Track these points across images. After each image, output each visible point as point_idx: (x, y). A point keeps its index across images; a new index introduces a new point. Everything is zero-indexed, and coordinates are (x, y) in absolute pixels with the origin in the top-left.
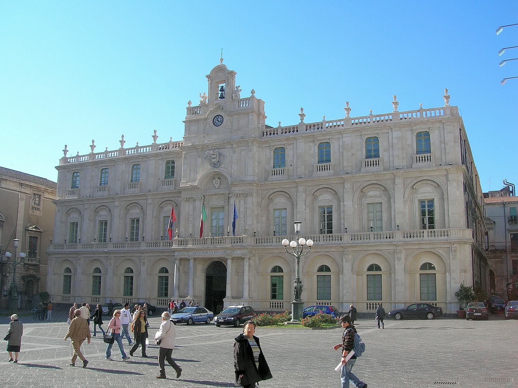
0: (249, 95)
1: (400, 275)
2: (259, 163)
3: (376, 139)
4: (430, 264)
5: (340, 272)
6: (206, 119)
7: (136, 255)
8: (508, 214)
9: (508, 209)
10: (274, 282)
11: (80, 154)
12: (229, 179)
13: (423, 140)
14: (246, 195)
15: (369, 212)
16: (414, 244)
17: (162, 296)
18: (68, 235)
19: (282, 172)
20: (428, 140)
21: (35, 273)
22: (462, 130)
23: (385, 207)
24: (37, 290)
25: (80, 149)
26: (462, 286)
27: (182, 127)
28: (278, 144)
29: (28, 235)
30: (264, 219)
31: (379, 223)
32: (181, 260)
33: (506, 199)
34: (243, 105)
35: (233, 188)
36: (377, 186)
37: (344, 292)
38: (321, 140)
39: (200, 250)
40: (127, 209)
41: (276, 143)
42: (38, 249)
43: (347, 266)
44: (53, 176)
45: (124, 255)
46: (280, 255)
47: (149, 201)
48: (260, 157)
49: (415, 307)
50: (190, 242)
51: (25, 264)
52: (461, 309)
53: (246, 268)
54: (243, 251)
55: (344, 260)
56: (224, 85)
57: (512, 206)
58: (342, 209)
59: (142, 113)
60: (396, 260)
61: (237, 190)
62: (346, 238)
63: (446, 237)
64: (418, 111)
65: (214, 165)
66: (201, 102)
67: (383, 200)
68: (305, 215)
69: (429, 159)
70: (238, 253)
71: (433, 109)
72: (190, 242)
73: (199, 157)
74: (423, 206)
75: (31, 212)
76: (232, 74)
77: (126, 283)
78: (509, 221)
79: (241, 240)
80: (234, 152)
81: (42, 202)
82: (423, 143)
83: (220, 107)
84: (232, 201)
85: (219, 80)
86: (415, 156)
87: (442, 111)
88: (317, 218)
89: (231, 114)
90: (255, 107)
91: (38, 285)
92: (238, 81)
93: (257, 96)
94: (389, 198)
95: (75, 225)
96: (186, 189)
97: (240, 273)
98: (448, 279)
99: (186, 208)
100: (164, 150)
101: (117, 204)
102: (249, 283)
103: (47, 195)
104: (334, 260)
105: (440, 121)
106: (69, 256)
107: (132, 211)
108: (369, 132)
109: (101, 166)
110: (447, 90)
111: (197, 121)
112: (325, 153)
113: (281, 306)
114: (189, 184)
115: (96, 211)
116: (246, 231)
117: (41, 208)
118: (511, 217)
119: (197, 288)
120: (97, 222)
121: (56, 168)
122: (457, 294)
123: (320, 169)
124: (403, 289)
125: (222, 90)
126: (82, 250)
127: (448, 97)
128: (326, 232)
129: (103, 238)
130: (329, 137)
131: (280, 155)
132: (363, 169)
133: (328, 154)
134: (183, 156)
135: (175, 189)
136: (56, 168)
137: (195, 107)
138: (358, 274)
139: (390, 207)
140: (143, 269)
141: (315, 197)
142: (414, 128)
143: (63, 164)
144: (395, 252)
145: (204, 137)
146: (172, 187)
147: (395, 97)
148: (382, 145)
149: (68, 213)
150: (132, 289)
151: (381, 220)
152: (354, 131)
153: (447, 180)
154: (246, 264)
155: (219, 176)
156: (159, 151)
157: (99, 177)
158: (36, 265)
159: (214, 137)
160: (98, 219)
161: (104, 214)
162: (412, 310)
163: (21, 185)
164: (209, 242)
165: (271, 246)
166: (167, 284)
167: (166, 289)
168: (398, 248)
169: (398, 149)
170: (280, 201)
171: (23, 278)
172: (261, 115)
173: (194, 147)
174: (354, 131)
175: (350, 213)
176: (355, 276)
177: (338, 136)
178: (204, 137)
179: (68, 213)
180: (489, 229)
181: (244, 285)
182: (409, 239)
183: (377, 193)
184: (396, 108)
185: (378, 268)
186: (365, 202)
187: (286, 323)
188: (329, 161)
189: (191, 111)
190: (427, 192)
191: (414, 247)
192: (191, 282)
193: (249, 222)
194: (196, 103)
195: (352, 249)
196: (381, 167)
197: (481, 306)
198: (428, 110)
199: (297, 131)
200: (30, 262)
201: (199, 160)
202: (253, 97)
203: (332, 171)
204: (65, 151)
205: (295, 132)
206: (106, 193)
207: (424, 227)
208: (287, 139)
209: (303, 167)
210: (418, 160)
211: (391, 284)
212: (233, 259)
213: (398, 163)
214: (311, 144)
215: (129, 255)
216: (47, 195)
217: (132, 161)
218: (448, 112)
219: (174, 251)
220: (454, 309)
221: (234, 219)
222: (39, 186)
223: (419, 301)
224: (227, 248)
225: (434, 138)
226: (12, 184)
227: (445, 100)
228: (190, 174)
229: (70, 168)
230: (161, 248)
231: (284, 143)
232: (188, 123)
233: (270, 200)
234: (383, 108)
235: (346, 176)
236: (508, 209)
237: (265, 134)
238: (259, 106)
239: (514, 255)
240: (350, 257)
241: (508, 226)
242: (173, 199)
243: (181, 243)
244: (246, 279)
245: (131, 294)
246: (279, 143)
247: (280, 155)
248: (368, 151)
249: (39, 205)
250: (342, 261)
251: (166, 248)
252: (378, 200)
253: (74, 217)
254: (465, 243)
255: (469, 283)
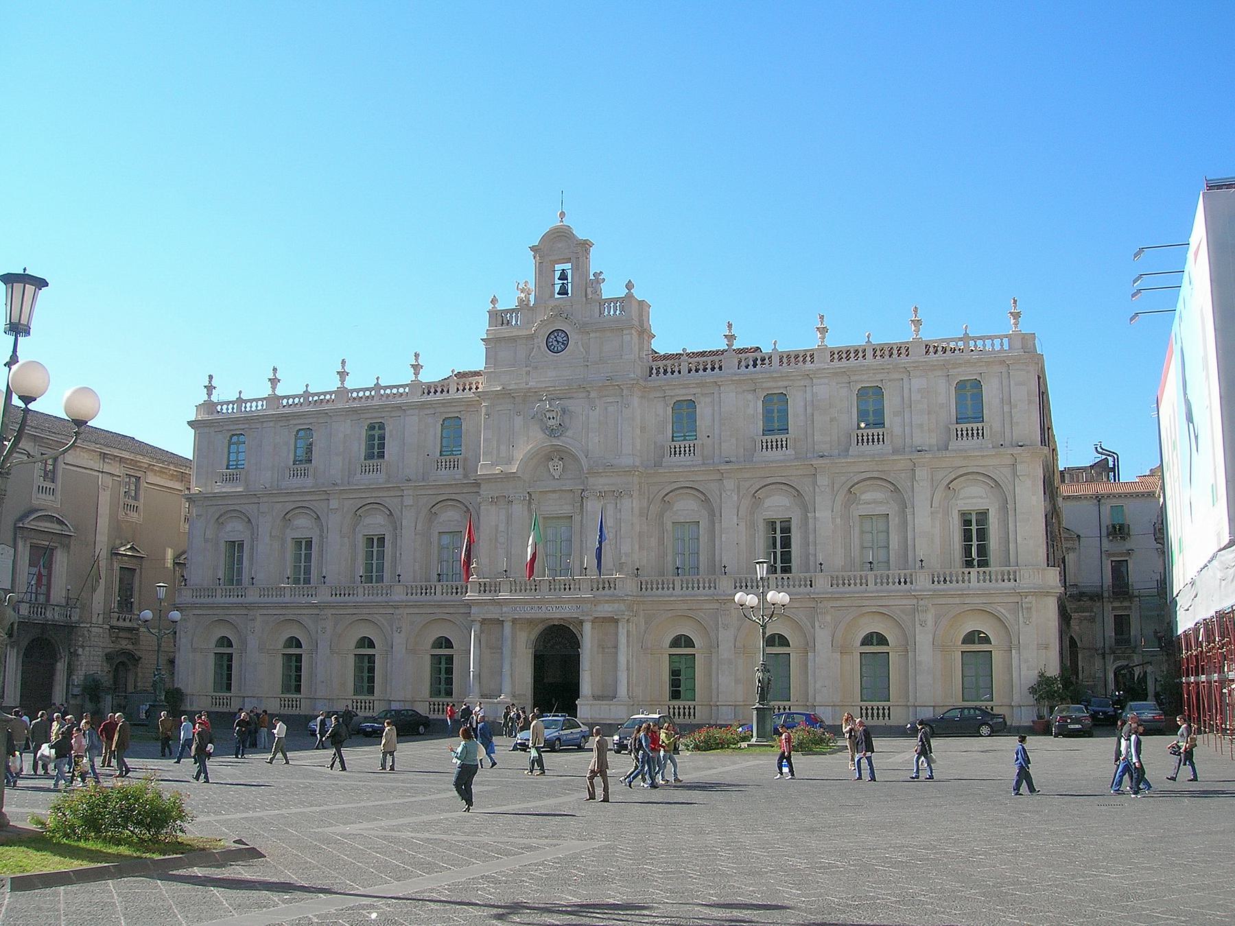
0: (623, 292)
1: (925, 653)
2: (643, 429)
3: (878, 391)
4: (781, 637)
5: (808, 647)
6: (531, 337)
7: (382, 611)
8: (1107, 521)
9: (1106, 509)
10: (676, 666)
11: (244, 397)
12: (584, 461)
13: (970, 397)
14: (618, 495)
15: (862, 532)
16: (952, 596)
17: (288, 691)
18: (222, 567)
19: (692, 450)
20: (978, 398)
21: (130, 647)
22: (1041, 379)
23: (894, 521)
24: (136, 681)
25: (245, 384)
26: (1042, 675)
27: (482, 348)
28: (682, 394)
29: (116, 566)
30: (654, 542)
31: (882, 552)
32: (483, 622)
33: (1102, 488)
34: (611, 312)
35: (591, 480)
36: (879, 482)
37: (817, 686)
38: (768, 389)
39: (526, 602)
40: (357, 515)
41: (677, 392)
42: (136, 594)
43: (822, 637)
44: (183, 444)
45: (355, 611)
46: (690, 614)
47: (408, 501)
48: (645, 419)
49: (957, 713)
50: (505, 587)
51: (112, 627)
52: (1040, 717)
53: (623, 640)
54: (616, 605)
55: (817, 624)
56: (568, 266)
57: (1115, 502)
58: (811, 526)
59: (395, 320)
60: (918, 626)
61: (600, 483)
62: (822, 583)
63: (1012, 583)
64: (961, 339)
65: (552, 432)
66: (521, 301)
67: (892, 509)
68: (738, 538)
69: (980, 434)
70: (606, 610)
71: (989, 338)
72: (505, 587)
73: (519, 413)
74: (967, 523)
75: (121, 514)
76: (586, 245)
77: (218, 665)
78: (1108, 535)
79: (611, 584)
80: (593, 408)
81: (142, 492)
82: (969, 402)
83: (560, 314)
84: (593, 506)
85: (556, 258)
86: (953, 427)
87: (1005, 341)
88: (762, 541)
89: (584, 328)
90: (632, 316)
91: (137, 674)
92: (596, 263)
93: (638, 294)
94: (903, 507)
95: (235, 547)
96: (490, 479)
97: (609, 649)
98: (1015, 663)
99: (490, 518)
100: (439, 396)
101: (334, 504)
102: (628, 669)
103: (152, 478)
104: (798, 626)
105: (1002, 362)
106: (229, 612)
107: (368, 521)
108: (865, 377)
109: (297, 427)
110: (1015, 302)
111: (514, 339)
112: (775, 414)
113: (691, 713)
114: (497, 470)
115: (286, 518)
116: (620, 567)
117: (141, 507)
118: (1114, 527)
119: (518, 676)
120: (289, 540)
121: (190, 423)
122: (1033, 690)
123: (767, 447)
124: (931, 681)
125: (563, 277)
126: (257, 599)
127: (1016, 316)
128: (779, 570)
129: (303, 575)
130: (786, 383)
131: (685, 413)
132: (854, 449)
133: (784, 414)
134: (483, 410)
135: (466, 476)
136: (190, 423)
137: (507, 311)
138: (844, 651)
139: (904, 523)
140: (399, 640)
141: (756, 499)
142: (952, 372)
143: (206, 417)
144: (915, 610)
145: (528, 373)
146: (458, 474)
147: (916, 309)
148: (890, 404)
149: (219, 522)
150: (229, 677)
151: (888, 547)
152: (836, 374)
153: (1015, 474)
154: (622, 631)
155: (560, 454)
156: (426, 398)
157: (292, 447)
158: (134, 629)
159: (551, 373)
160: (291, 534)
161: (303, 526)
162: (952, 720)
163: (104, 456)
164: (545, 587)
165: (671, 596)
166: (449, 671)
167: (449, 681)
168: (921, 603)
169: (918, 410)
170: (687, 508)
171: (109, 657)
172: (645, 333)
173: (506, 394)
174: (836, 374)
175: (827, 533)
176: (838, 656)
177: (802, 383)
178: (528, 373)
179: (219, 522)
180: (1068, 549)
181: (619, 673)
182: (942, 586)
183: (879, 495)
184: (917, 331)
185: (882, 640)
186: (856, 513)
187: (744, 745)
188: (785, 430)
189: (499, 318)
190: (975, 497)
191: (951, 601)
192: (506, 669)
193: (625, 548)
194: (508, 302)
195: (832, 604)
196: (887, 447)
197: (1078, 712)
198: (979, 338)
199: (720, 368)
200: (121, 624)
201: (518, 421)
202: (630, 296)
203: (790, 452)
204: (210, 389)
205: (717, 370)
206: (309, 482)
207: (969, 564)
208: (702, 385)
209: (734, 440)
210: (960, 435)
211: (806, 665)
212: (595, 621)
213: (919, 439)
214: (750, 396)
215: (365, 611)
216: (152, 478)
217: (369, 415)
218: (1018, 344)
219: (469, 605)
220: (1026, 717)
221: (600, 543)
222: (139, 458)
223: (961, 704)
224: (584, 601)
225: (991, 393)
226: (86, 455)
227: (1012, 321)
228: (498, 450)
229: (220, 427)
230: (438, 597)
231: (695, 391)
232: (492, 343)
233: (666, 502)
234: (893, 330)
235: (821, 461)
236: (1106, 509)
237: (654, 371)
238: (641, 315)
239: (1116, 604)
240: (828, 618)
241: (1106, 545)
242: (466, 496)
243: (483, 588)
244: (622, 659)
245: (229, 688)
246: (684, 391)
247: (685, 413)
248: (862, 415)
249: (136, 498)
250: (813, 627)
251: (449, 597)
252: (881, 510)
253: (235, 530)
254: (1047, 594)
255: (1053, 670)
